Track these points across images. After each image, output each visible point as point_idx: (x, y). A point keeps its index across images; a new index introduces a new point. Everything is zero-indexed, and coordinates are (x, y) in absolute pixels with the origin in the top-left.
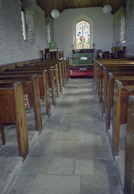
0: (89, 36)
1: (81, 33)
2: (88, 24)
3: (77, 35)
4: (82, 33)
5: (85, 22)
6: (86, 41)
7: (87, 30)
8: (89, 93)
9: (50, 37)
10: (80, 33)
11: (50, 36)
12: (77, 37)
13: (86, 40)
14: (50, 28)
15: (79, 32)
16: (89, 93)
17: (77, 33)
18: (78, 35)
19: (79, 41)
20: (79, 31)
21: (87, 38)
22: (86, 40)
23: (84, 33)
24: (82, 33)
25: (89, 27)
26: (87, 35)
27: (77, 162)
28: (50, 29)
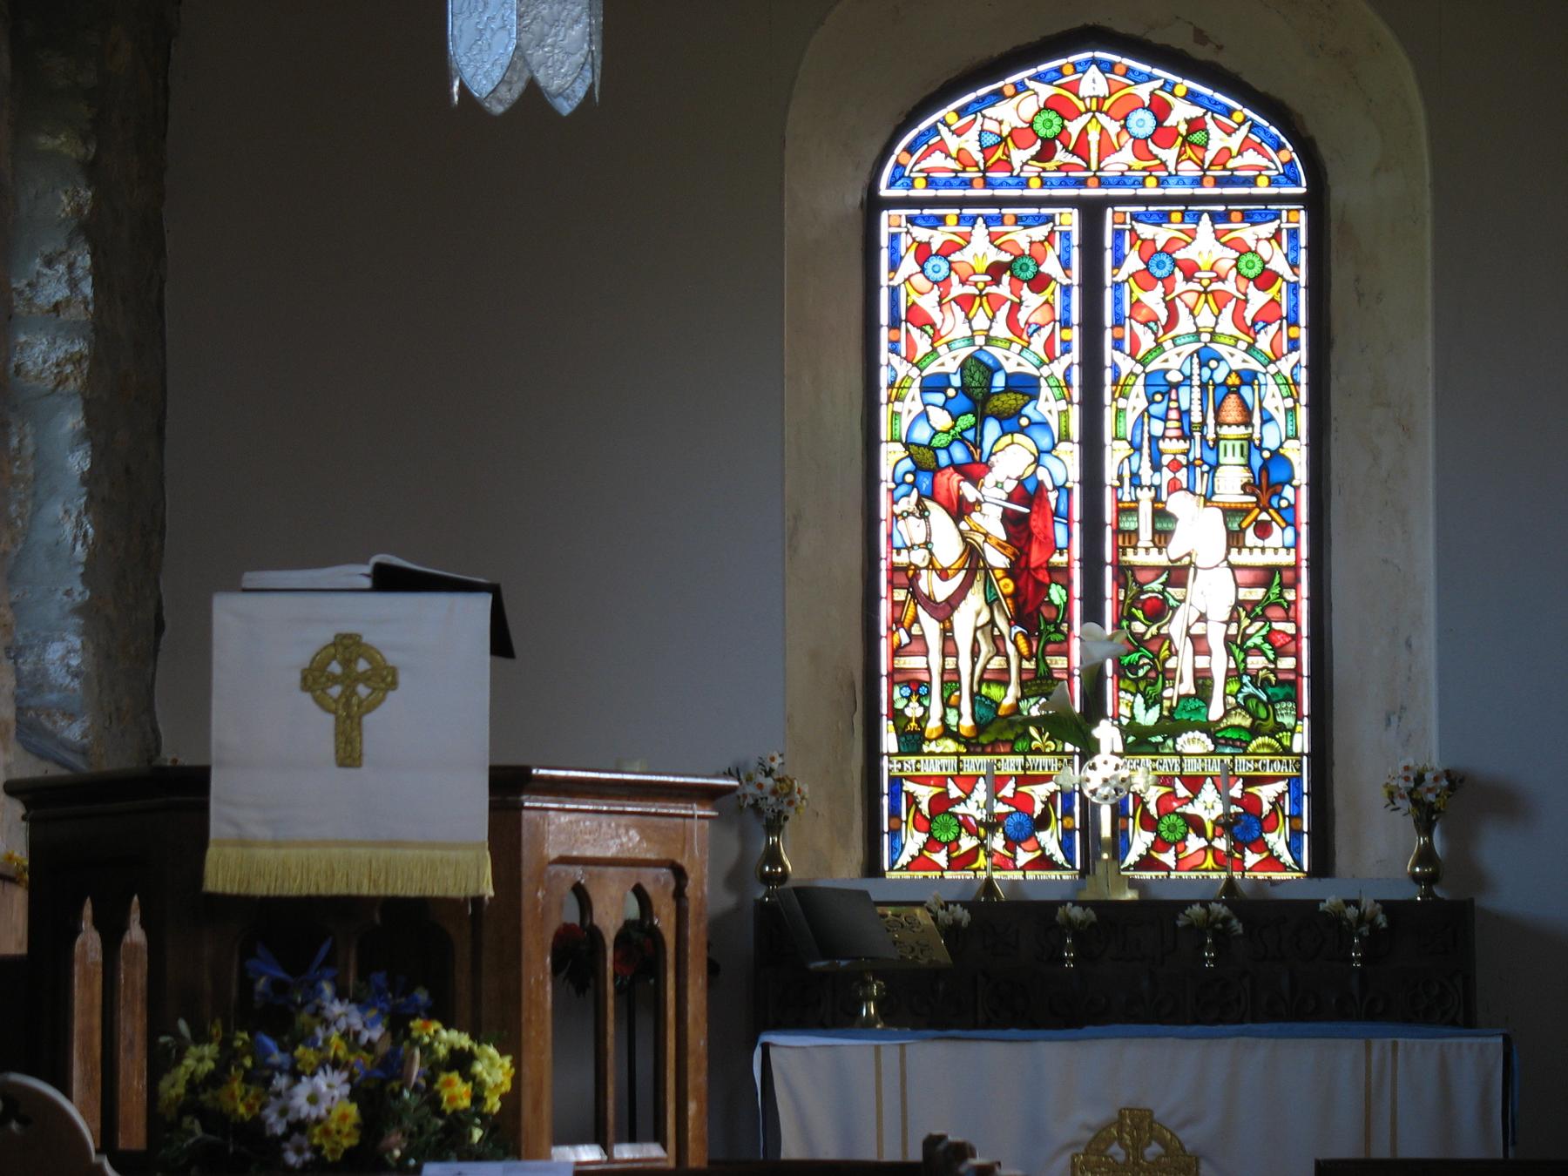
0: (1297, 494)
1: (1047, 406)
2: (1242, 145)
3: (891, 457)
4: (1053, 408)
5: (1151, 81)
6: (1184, 663)
7: (1224, 293)
8: (112, 935)
9: (78, 462)
10: (986, 397)
11: (72, 420)
12: (923, 538)
13: (1211, 596)
14: (92, 170)
15: (979, 368)
16: (112, 935)
17: (911, 416)
18: (942, 476)
19: (953, 643)
20: (956, 338)
21: (1211, 567)
22: (1211, 596)
23: (1125, 411)
24: (1053, 408)
25: (1277, 246)
26: (1231, 482)
27: (1501, 1156)
28: (90, 229)
